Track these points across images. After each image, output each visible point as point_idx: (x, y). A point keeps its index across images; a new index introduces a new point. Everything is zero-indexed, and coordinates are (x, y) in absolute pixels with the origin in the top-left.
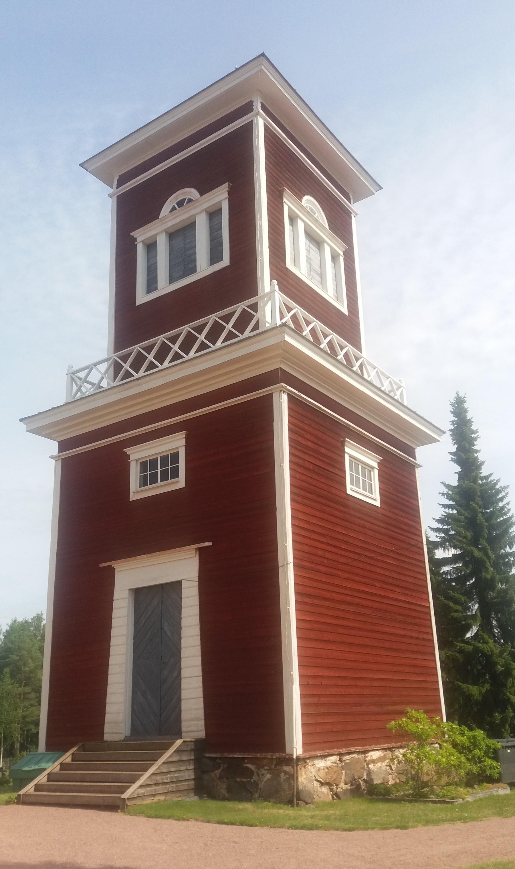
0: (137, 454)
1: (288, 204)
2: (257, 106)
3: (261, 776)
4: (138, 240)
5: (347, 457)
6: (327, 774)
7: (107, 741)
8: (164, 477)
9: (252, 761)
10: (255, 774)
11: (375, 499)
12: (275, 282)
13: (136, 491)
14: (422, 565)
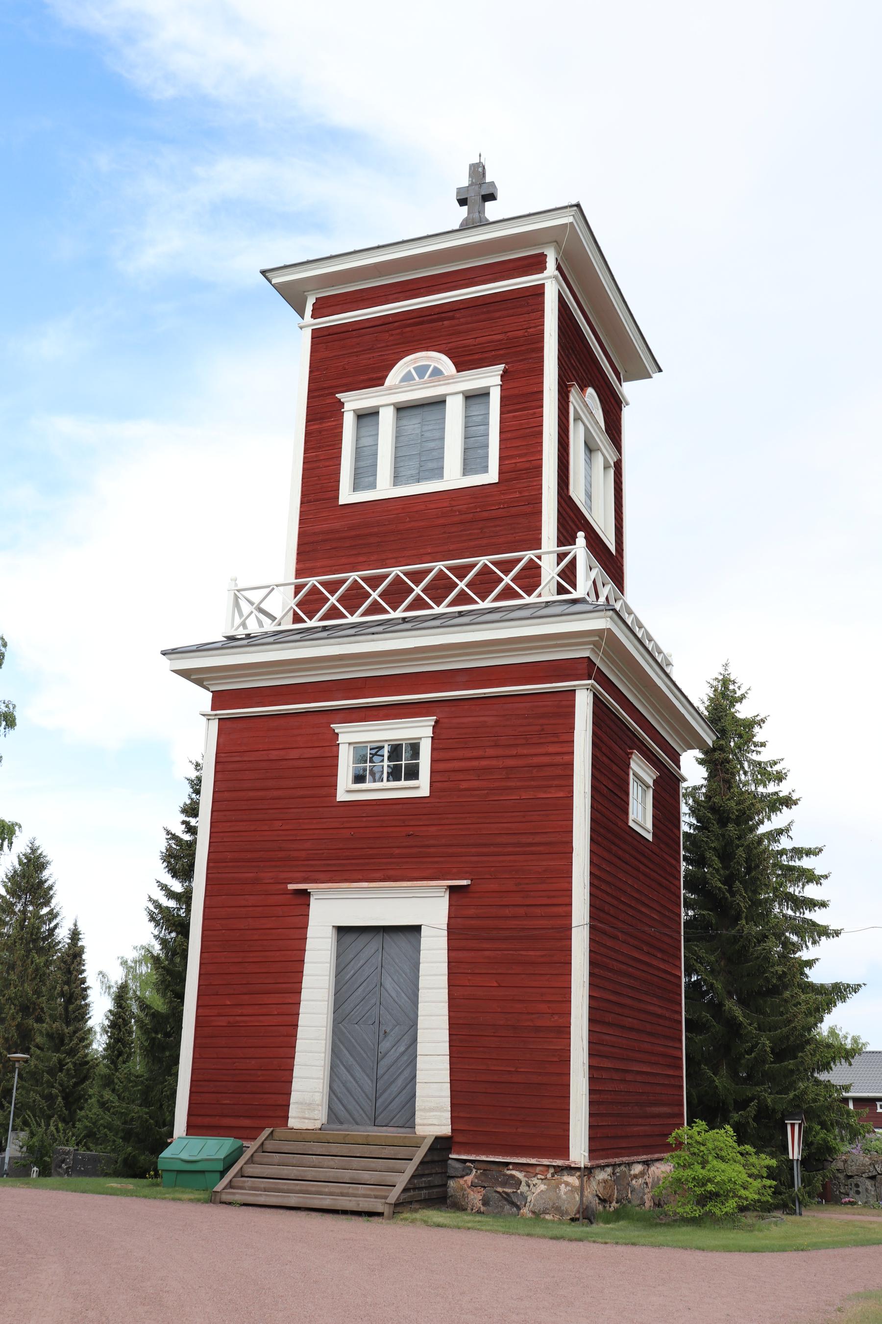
0: (350, 736)
3: (532, 1186)
4: (347, 407)
7: (292, 1129)
8: (395, 774)
10: (523, 1183)
13: (345, 789)
14: (677, 919)
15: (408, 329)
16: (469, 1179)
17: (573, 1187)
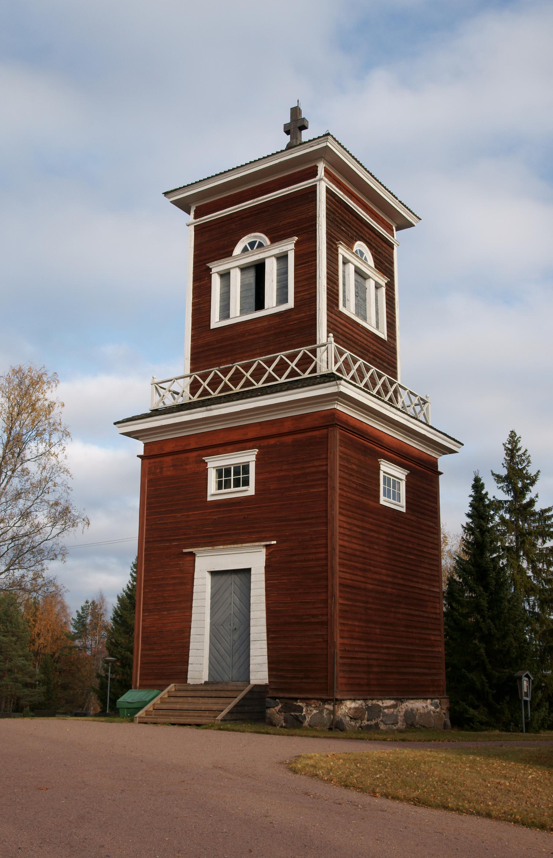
1: (342, 251)
2: (321, 172)
4: (214, 270)
5: (382, 474)
6: (355, 712)
8: (237, 485)
9: (302, 700)
11: (401, 506)
12: (331, 335)
15: (245, 220)
16: (277, 708)
17: (330, 711)
